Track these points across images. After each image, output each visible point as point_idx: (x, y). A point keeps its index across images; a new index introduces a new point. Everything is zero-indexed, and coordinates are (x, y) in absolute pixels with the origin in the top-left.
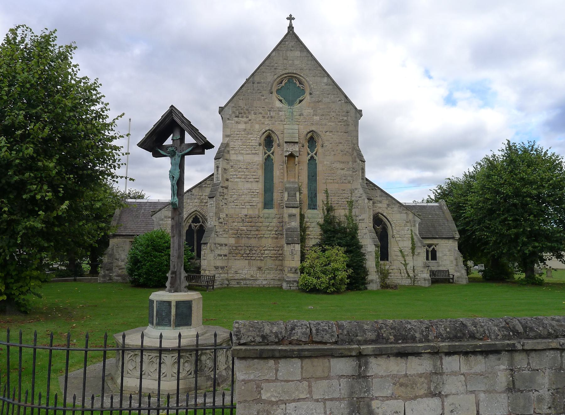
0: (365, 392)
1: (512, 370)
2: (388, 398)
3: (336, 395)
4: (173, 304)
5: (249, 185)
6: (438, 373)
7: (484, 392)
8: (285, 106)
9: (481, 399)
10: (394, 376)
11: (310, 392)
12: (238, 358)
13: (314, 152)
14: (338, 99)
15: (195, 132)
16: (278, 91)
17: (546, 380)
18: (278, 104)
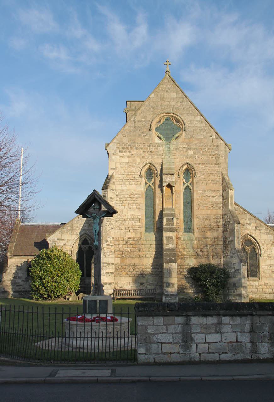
0: (189, 330)
1: (252, 323)
2: (198, 333)
3: (178, 331)
4: (98, 301)
5: (131, 212)
6: (220, 323)
7: (240, 332)
8: (163, 142)
9: (238, 335)
10: (201, 324)
11: (167, 330)
12: (165, 231)
13: (189, 182)
14: (209, 135)
15: (107, 205)
16: (157, 129)
17: (267, 328)
18: (157, 140)
